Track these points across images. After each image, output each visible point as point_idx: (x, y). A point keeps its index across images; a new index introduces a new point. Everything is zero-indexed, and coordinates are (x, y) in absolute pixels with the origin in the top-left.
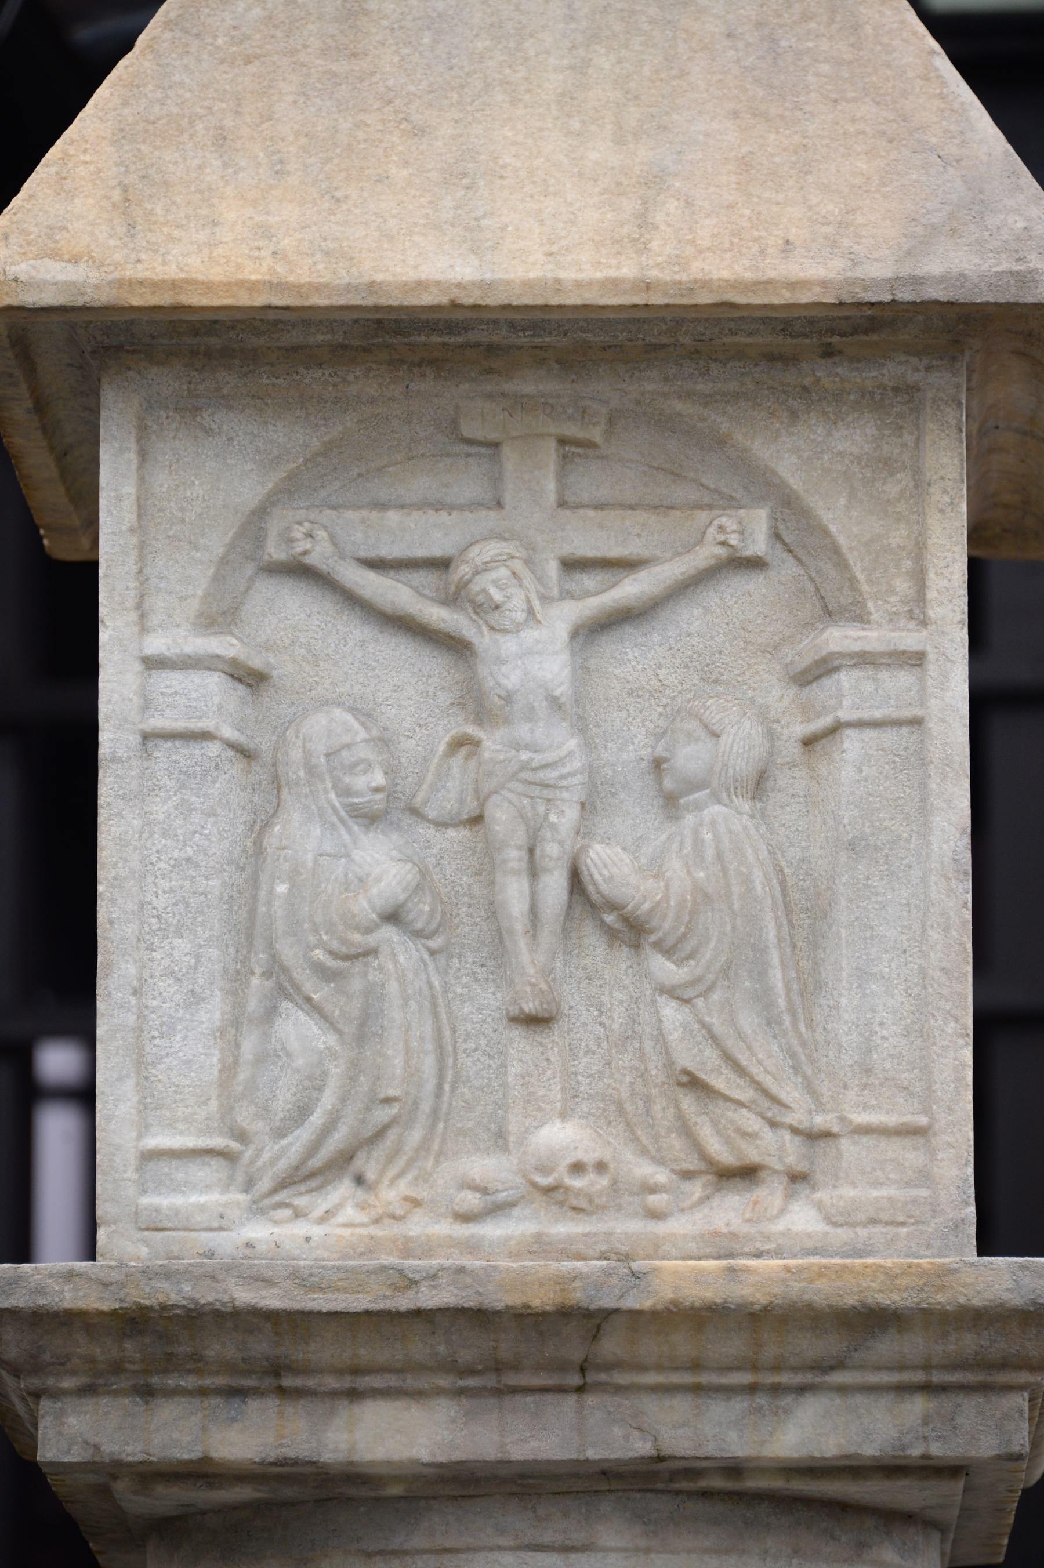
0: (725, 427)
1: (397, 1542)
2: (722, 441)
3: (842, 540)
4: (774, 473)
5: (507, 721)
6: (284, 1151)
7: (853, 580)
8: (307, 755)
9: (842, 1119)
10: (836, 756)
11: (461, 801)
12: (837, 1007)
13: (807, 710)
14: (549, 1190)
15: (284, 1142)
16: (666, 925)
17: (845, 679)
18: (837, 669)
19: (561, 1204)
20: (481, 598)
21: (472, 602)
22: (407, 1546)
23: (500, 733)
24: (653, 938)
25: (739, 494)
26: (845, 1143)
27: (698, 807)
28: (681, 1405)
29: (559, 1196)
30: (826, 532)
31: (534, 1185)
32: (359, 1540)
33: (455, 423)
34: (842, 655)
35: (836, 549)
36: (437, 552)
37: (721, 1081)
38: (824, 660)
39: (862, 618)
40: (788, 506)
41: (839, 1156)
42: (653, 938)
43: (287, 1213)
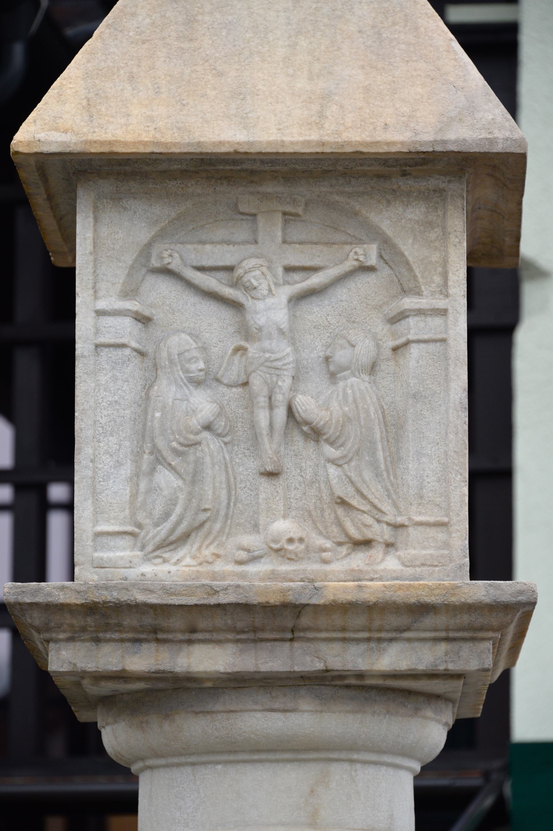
0: (357, 208)
1: (209, 707)
2: (356, 214)
3: (410, 259)
4: (380, 228)
5: (259, 340)
6: (158, 532)
7: (415, 277)
8: (170, 354)
9: (409, 519)
10: (407, 356)
11: (239, 375)
12: (407, 468)
13: (394, 335)
14: (278, 551)
15: (158, 529)
16: (331, 432)
17: (412, 321)
18: (408, 317)
19: (283, 557)
20: (248, 284)
21: (244, 286)
22: (214, 709)
23: (257, 345)
24: (325, 437)
25: (364, 238)
26: (411, 530)
27: (345, 378)
28: (337, 647)
29: (282, 553)
30: (403, 255)
31: (271, 548)
32: (192, 706)
33: (236, 205)
34: (410, 310)
35: (407, 263)
36: (228, 263)
37: (355, 502)
38: (402, 313)
39: (419, 294)
40: (386, 244)
41: (408, 535)
42: (325, 437)
43: (160, 560)
